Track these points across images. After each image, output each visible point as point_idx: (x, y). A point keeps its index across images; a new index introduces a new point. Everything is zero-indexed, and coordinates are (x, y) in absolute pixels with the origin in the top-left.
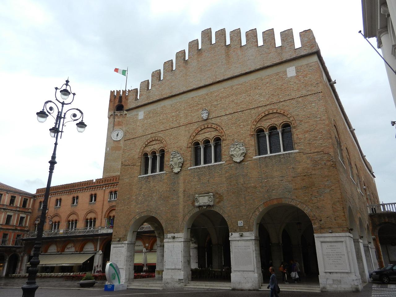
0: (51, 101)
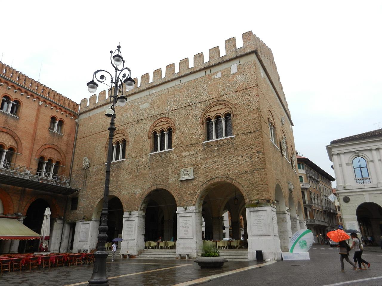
0: (101, 71)
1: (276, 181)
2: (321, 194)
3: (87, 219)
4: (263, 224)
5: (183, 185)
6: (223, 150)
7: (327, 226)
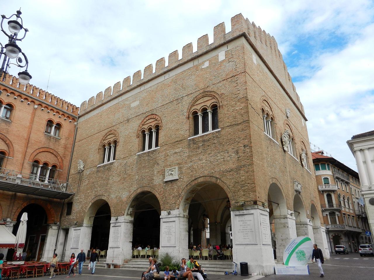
1: (270, 180)
2: (353, 196)
3: (79, 224)
4: (249, 230)
5: (167, 187)
6: (208, 146)
7: (361, 233)
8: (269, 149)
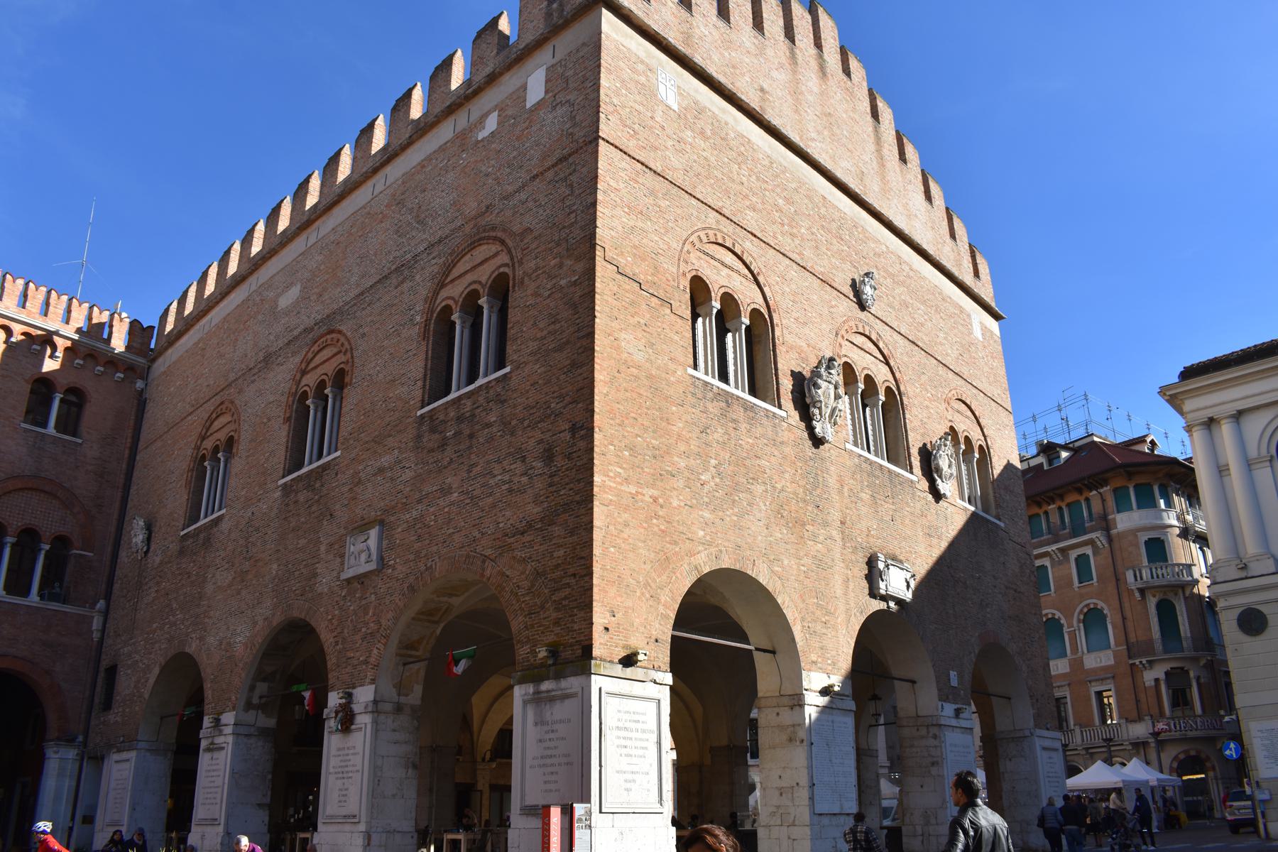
8: (718, 434)
